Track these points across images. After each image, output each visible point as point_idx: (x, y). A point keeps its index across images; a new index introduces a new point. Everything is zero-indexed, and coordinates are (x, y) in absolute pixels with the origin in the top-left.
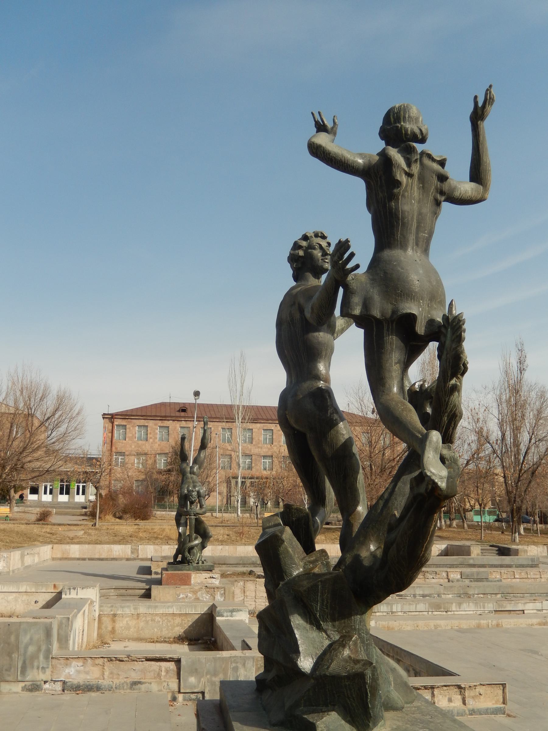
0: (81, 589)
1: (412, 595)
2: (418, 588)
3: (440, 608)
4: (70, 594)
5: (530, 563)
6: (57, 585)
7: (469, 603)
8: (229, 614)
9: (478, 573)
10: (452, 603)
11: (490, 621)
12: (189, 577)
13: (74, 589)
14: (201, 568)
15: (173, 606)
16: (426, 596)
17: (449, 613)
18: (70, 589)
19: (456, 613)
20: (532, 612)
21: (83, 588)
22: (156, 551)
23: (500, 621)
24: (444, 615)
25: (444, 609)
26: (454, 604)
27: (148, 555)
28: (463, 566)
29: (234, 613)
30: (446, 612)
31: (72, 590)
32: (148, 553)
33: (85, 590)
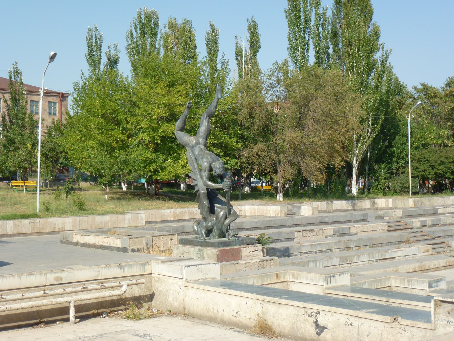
0: (339, 275)
1: (314, 252)
2: (318, 245)
3: (347, 261)
4: (331, 283)
5: (362, 218)
6: (279, 275)
7: (364, 255)
8: (436, 284)
9: (343, 229)
10: (354, 256)
11: (392, 269)
12: (239, 251)
13: (334, 276)
14: (245, 241)
15: (366, 283)
16: (323, 252)
17: (352, 264)
18: (330, 277)
19: (356, 264)
20: (400, 258)
21: (340, 275)
22: (16, 226)
23: (398, 267)
24: (349, 266)
25: (350, 262)
26: (356, 257)
27: (8, 231)
28: (321, 223)
29: (439, 283)
30: (350, 264)
31: (332, 278)
32: (8, 229)
33: (342, 276)
